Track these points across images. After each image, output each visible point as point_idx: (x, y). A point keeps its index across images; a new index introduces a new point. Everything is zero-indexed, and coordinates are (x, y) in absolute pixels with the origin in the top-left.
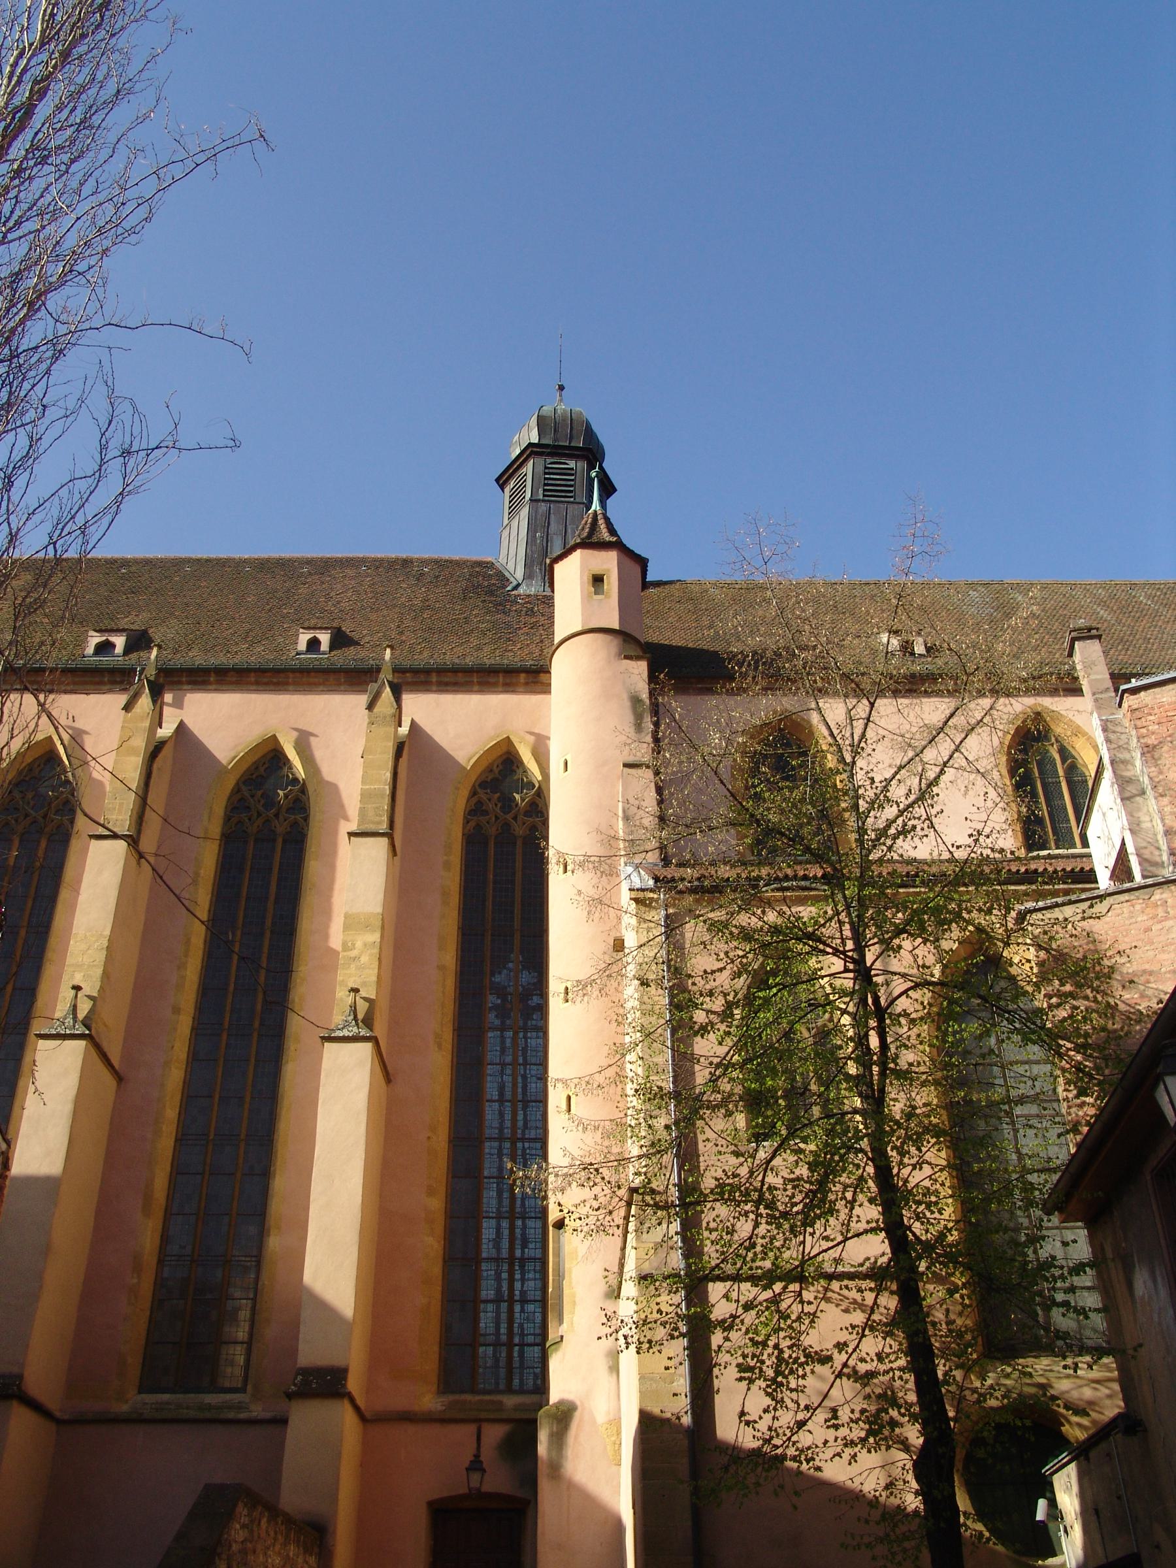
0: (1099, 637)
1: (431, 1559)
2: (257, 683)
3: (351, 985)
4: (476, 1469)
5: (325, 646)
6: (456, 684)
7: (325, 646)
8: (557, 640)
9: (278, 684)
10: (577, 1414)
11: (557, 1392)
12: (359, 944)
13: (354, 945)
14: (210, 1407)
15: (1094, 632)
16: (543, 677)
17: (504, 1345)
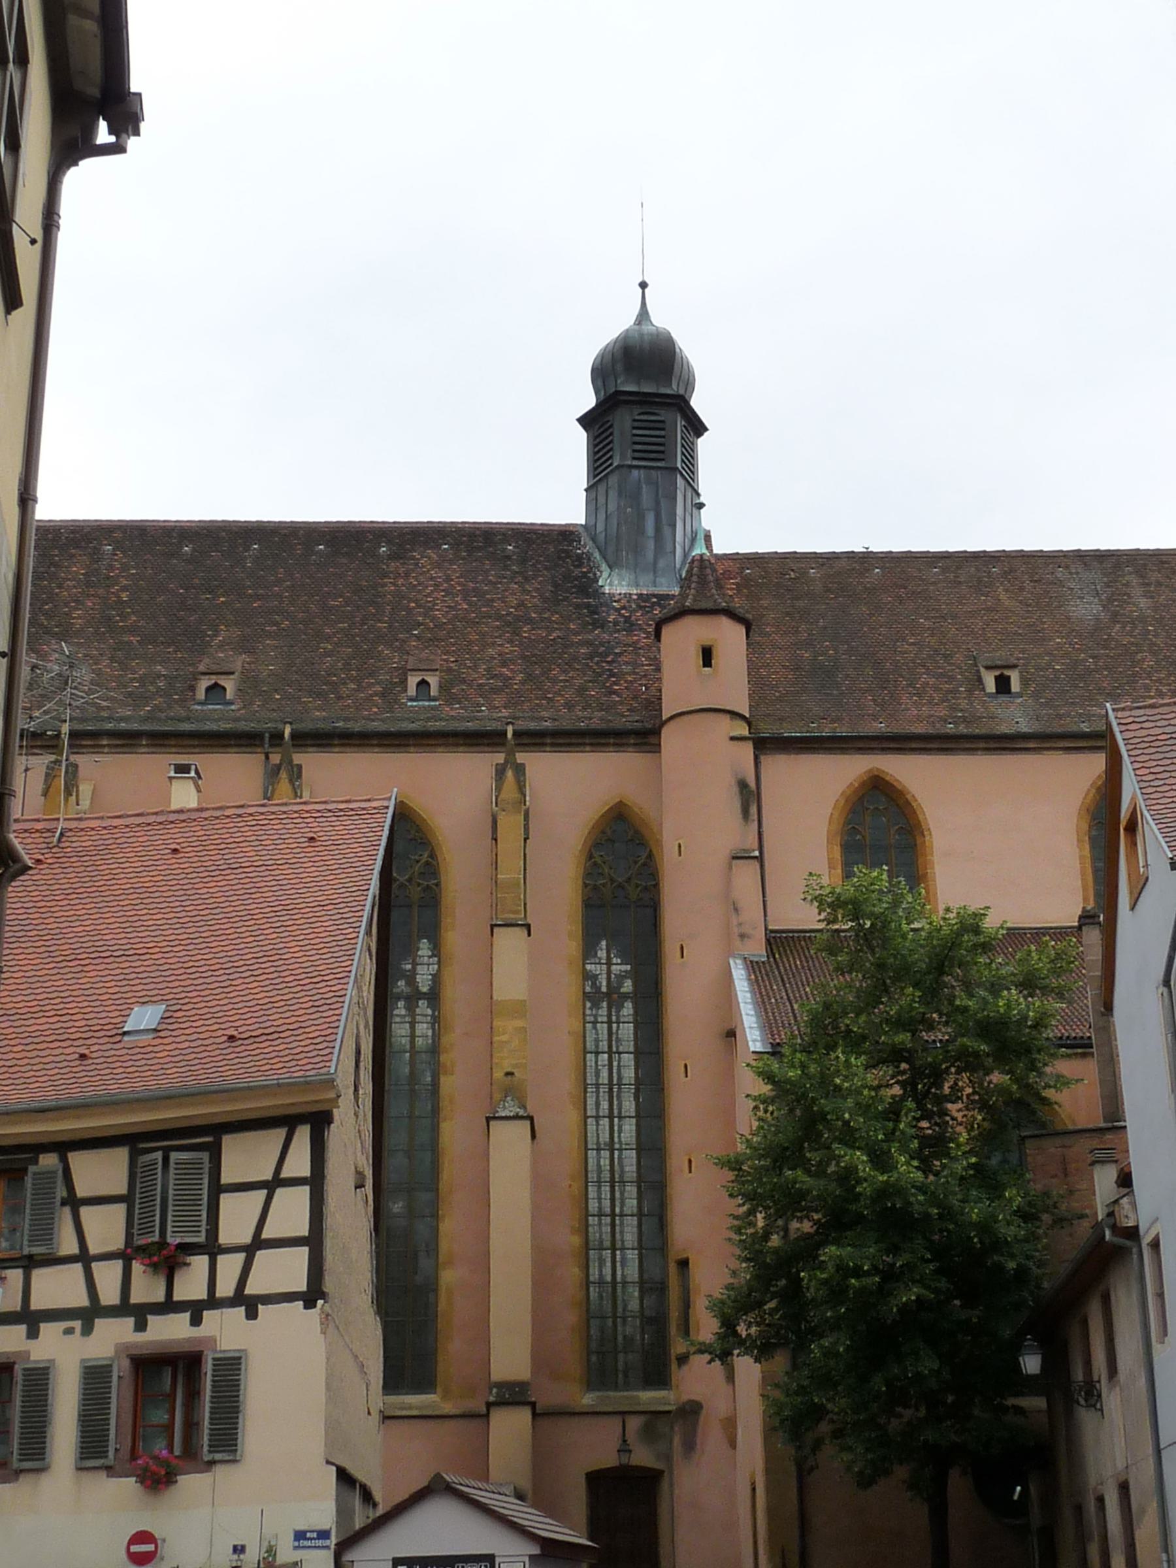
5: (434, 691)
6: (570, 745)
14: (410, 1408)
16: (653, 740)
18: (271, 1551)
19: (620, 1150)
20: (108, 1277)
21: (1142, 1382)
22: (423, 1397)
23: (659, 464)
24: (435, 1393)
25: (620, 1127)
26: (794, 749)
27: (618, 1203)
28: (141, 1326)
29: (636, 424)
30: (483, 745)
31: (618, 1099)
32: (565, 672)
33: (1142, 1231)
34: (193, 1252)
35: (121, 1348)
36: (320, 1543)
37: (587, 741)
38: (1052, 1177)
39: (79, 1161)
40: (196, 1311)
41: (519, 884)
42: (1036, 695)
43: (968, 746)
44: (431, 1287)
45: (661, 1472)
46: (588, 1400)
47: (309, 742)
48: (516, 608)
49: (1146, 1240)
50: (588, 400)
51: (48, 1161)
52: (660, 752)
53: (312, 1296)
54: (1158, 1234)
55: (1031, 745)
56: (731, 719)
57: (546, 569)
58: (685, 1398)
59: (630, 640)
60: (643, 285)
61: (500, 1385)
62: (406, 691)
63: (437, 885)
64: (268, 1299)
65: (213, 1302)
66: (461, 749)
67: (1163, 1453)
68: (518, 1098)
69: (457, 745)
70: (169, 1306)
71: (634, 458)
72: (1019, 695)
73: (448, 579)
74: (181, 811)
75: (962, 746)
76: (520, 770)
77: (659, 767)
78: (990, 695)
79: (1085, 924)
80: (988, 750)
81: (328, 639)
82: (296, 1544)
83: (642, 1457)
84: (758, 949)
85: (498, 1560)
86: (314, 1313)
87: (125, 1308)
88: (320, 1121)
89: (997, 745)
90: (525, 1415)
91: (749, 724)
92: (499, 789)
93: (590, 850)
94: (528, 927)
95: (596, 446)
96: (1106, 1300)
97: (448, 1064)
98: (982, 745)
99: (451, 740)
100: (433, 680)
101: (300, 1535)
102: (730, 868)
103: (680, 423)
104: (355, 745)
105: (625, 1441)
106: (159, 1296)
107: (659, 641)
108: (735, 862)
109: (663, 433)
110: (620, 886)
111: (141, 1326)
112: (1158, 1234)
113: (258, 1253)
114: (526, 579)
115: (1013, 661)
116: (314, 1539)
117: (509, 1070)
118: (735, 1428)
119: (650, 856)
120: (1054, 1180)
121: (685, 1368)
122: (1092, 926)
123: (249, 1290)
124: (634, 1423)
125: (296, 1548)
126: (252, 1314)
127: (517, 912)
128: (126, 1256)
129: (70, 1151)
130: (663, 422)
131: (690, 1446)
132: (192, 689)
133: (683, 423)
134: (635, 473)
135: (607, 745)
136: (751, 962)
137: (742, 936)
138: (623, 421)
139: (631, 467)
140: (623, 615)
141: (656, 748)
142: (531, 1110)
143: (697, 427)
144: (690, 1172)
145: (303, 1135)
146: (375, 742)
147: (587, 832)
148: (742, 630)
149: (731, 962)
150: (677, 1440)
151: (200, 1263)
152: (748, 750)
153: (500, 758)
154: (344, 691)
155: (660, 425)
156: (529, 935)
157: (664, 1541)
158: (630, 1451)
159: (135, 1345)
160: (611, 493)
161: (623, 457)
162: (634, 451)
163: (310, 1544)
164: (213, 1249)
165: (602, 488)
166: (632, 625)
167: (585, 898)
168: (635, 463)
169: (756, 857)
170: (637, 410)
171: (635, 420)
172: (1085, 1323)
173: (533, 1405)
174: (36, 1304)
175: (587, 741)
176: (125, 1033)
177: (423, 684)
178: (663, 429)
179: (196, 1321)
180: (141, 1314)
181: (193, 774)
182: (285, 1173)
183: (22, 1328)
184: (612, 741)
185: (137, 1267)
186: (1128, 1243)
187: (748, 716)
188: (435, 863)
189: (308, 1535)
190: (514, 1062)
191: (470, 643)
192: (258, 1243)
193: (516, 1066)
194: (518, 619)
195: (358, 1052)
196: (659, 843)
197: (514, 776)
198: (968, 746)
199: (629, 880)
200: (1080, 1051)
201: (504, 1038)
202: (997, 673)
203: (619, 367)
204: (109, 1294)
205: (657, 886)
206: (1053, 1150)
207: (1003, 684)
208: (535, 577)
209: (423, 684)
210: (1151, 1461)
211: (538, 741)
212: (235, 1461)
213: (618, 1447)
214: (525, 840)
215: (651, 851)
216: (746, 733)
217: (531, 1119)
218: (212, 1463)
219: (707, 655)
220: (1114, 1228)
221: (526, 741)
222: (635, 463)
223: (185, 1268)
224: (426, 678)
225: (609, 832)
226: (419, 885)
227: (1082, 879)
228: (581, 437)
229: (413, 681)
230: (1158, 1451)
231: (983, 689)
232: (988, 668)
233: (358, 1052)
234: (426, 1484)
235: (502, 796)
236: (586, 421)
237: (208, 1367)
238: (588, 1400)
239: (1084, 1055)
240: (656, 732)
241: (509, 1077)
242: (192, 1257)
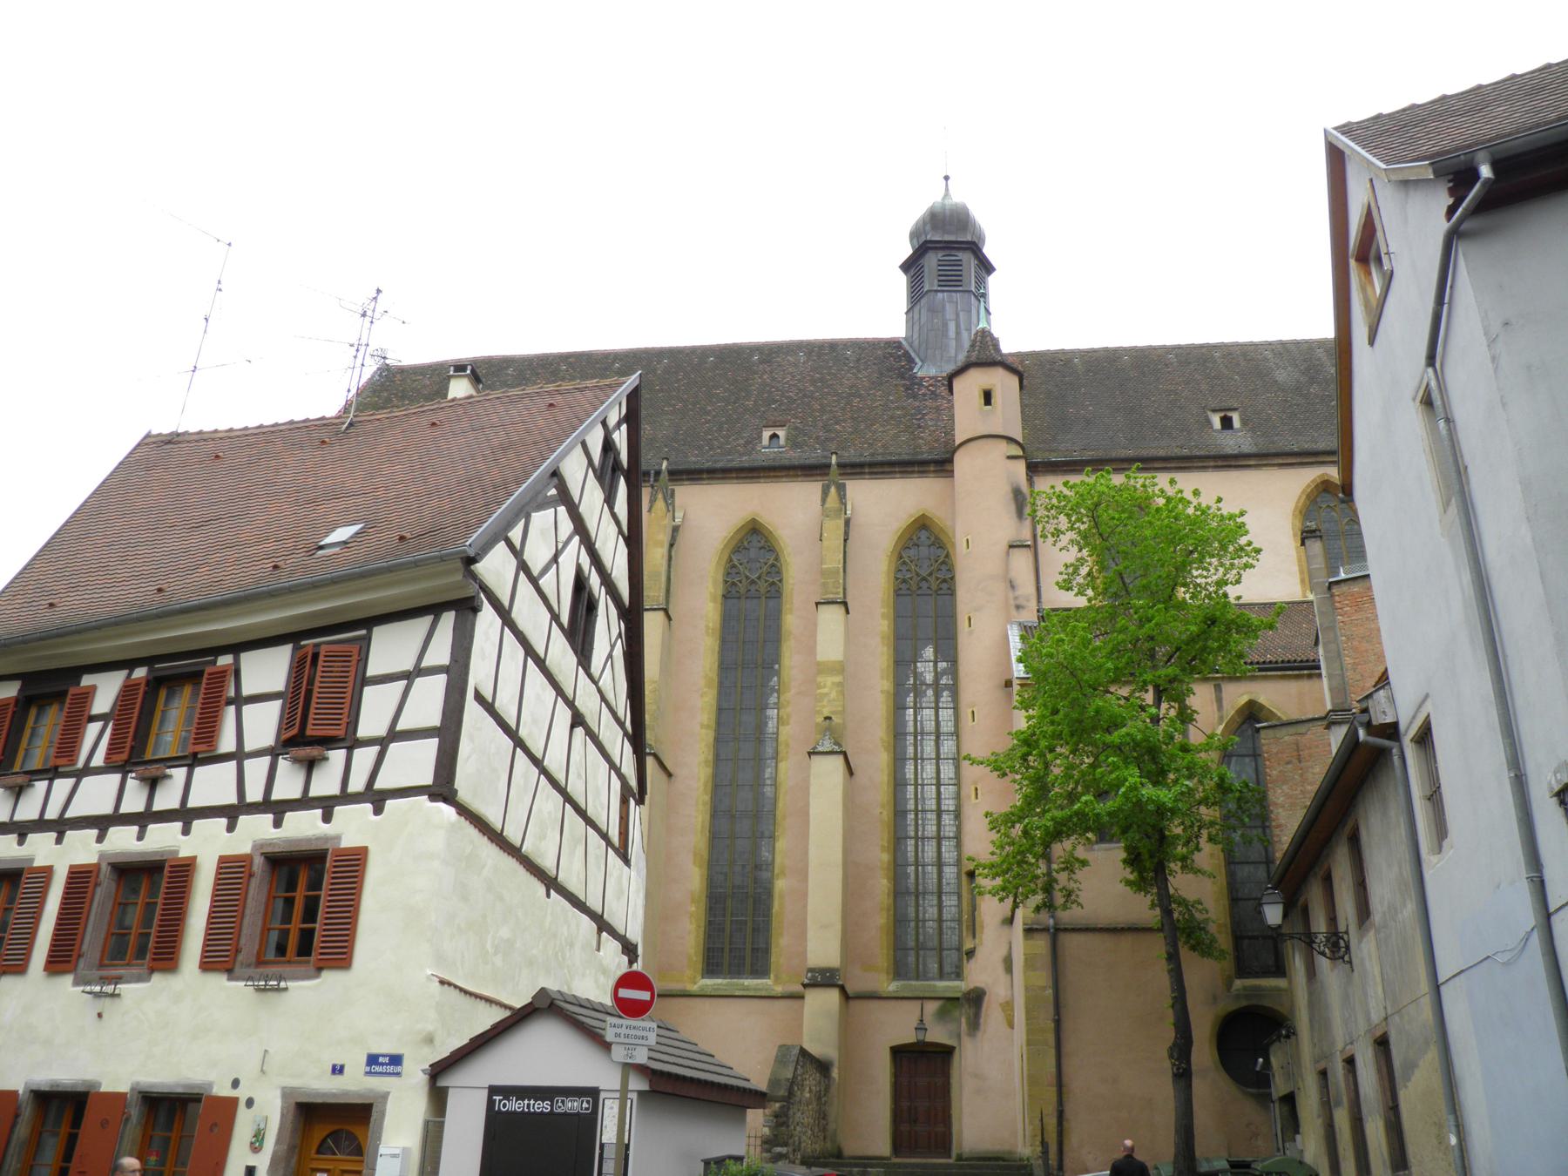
0: (1321, 537)
1: (893, 1080)
2: (737, 478)
3: (826, 714)
4: (921, 1029)
5: (782, 441)
6: (883, 473)
7: (782, 441)
8: (957, 443)
9: (753, 478)
10: (986, 998)
11: (123, 988)
12: (829, 684)
13: (825, 684)
14: (747, 989)
15: (1318, 533)
16: (948, 467)
17: (912, 949)
19: (923, 785)
20: (256, 770)
21: (1410, 909)
22: (759, 981)
23: (960, 289)
24: (769, 978)
25: (922, 767)
26: (1061, 471)
27: (920, 828)
28: (277, 824)
29: (940, 263)
30: (817, 475)
32: (883, 426)
33: (1402, 727)
34: (332, 746)
35: (257, 846)
36: (390, 1069)
37: (897, 470)
38: (1288, 763)
39: (249, 660)
40: (327, 806)
41: (838, 572)
42: (1253, 430)
43: (1200, 464)
44: (769, 893)
45: (953, 1048)
46: (893, 987)
47: (684, 477)
49: (1409, 733)
50: (906, 251)
52: (953, 477)
53: (442, 789)
54: (1429, 715)
55: (1252, 463)
56: (1007, 443)
57: (874, 364)
59: (934, 405)
60: (947, 178)
61: (811, 970)
62: (761, 443)
63: (780, 581)
65: (345, 798)
66: (799, 479)
67: (1443, 989)
68: (834, 738)
69: (798, 476)
70: (304, 802)
71: (939, 286)
72: (1239, 430)
74: (453, 400)
75: (1195, 465)
76: (841, 489)
77: (953, 486)
78: (1216, 431)
79: (1307, 538)
80: (1217, 468)
81: (708, 413)
82: (368, 1069)
83: (938, 1034)
84: (1030, 617)
85: (603, 1095)
89: (1225, 464)
90: (833, 996)
91: (1023, 449)
92: (824, 500)
93: (900, 553)
94: (845, 604)
95: (912, 287)
96: (1355, 841)
97: (785, 717)
98: (1212, 464)
99: (791, 473)
100: (781, 433)
101: (372, 1060)
102: (1008, 554)
103: (974, 262)
104: (719, 479)
105: (922, 1021)
106: (295, 793)
107: (952, 394)
108: (1011, 550)
109: (960, 268)
110: (924, 579)
111: (277, 824)
112: (1429, 715)
113: (392, 745)
114: (859, 371)
115: (1236, 405)
116: (386, 1064)
117: (829, 715)
118: (1012, 1010)
119: (947, 556)
120: (1290, 766)
121: (972, 962)
122: (1313, 540)
124: (931, 1007)
125: (368, 1073)
126: (378, 810)
127: (838, 593)
128: (274, 753)
129: (243, 652)
130: (960, 260)
131: (975, 1025)
133: (976, 262)
134: (940, 295)
135: (913, 472)
136: (1025, 627)
137: (1018, 607)
138: (932, 261)
139: (937, 291)
140: (930, 390)
141: (950, 473)
143: (986, 267)
144: (977, 798)
146: (734, 475)
147: (896, 538)
148: (1014, 381)
149: (1009, 627)
151: (337, 756)
152: (1020, 468)
155: (958, 263)
156: (847, 612)
158: (926, 1029)
159: (270, 843)
160: (922, 311)
161: (931, 285)
162: (939, 281)
163: (381, 1070)
164: (352, 743)
165: (916, 309)
166: (936, 396)
167: (896, 588)
168: (939, 288)
169: (1029, 546)
170: (940, 255)
171: (939, 260)
172: (1328, 880)
173: (842, 989)
174: (192, 803)
175: (897, 470)
176: (321, 548)
177: (774, 436)
178: (961, 265)
179: (327, 818)
180: (277, 809)
181: (468, 372)
182: (425, 663)
183: (178, 825)
184: (916, 469)
185: (283, 764)
186: (1386, 743)
187: (1021, 442)
188: (778, 564)
189: (381, 1060)
190: (834, 709)
191: (814, 410)
192: (394, 735)
193: (834, 712)
194: (851, 395)
196: (953, 545)
197: (837, 491)
198: (1200, 464)
199: (930, 574)
200: (1306, 672)
201: (825, 690)
202: (1222, 414)
203: (928, 227)
204: (254, 794)
205: (952, 578)
206: (1286, 738)
207: (1227, 423)
208: (866, 369)
209: (774, 436)
210: (1427, 1003)
211: (858, 470)
212: (398, 1074)
213: (915, 1025)
214: (845, 540)
215: (948, 552)
216: (1021, 453)
217: (845, 754)
219: (988, 397)
220: (1368, 725)
221: (849, 471)
222: (939, 288)
223: (323, 763)
224: (777, 432)
225: (915, 538)
226: (766, 581)
227: (1299, 565)
228: (902, 280)
229: (766, 434)
230: (1437, 988)
231: (1212, 428)
232: (1214, 411)
234: (530, 1000)
235: (827, 505)
236: (906, 267)
238: (893, 987)
239: (1310, 676)
240: (950, 461)
241: (828, 721)
242: (330, 752)
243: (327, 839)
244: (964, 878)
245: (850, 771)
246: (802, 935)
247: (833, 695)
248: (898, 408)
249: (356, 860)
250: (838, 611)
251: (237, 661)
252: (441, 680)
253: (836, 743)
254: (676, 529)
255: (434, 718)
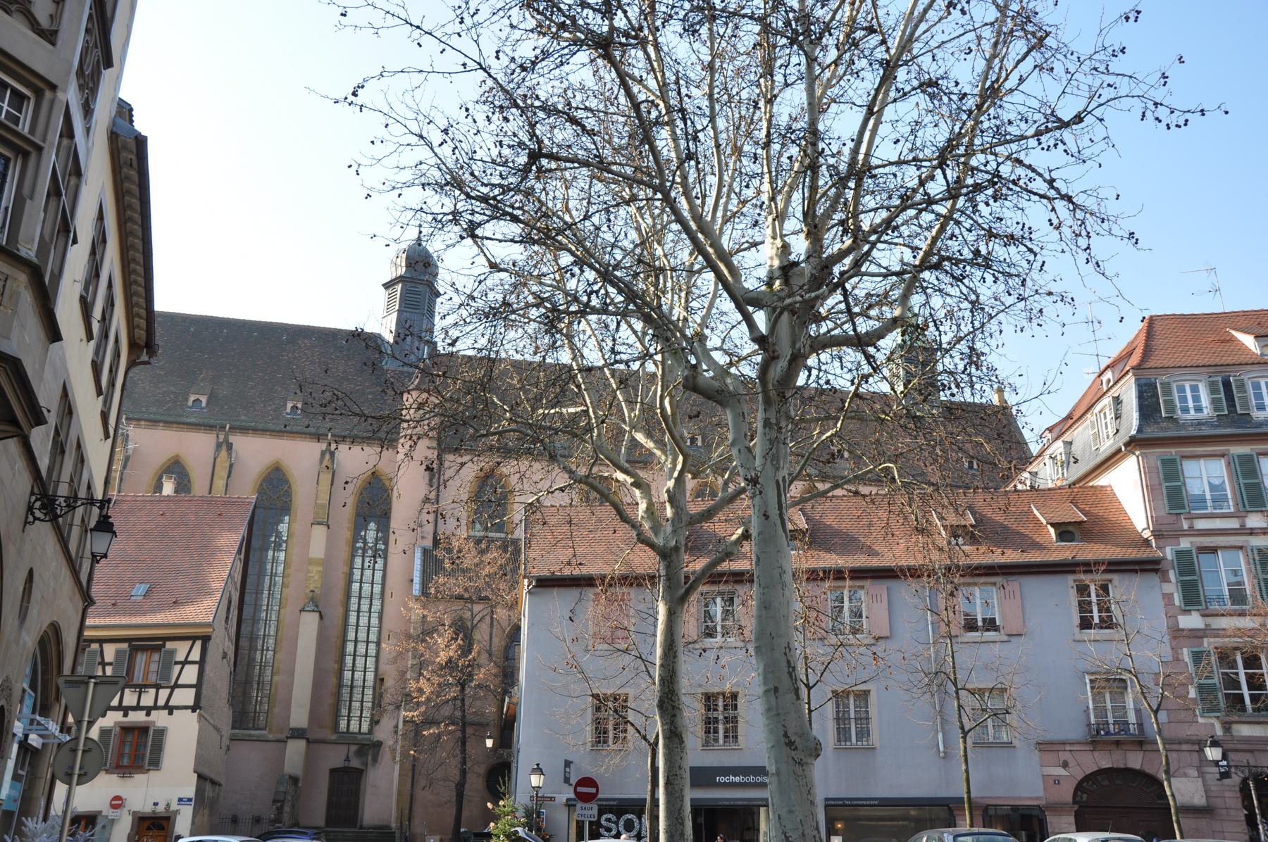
18: (168, 805)
28: (126, 715)
31: (722, 261)
35: (116, 723)
40: (148, 710)
48: (343, 373)
51: (95, 646)
58: (376, 739)
61: (291, 729)
64: (178, 708)
65: (156, 707)
70: (138, 708)
73: (313, 356)
83: (355, 763)
86: (195, 714)
87: (120, 707)
88: (206, 639)
90: (301, 744)
92: (321, 462)
101: (180, 800)
106: (135, 704)
111: (126, 715)
123: (171, 703)
124: (354, 748)
126: (171, 713)
131: (375, 760)
132: (187, 400)
142: (320, 609)
145: (198, 644)
150: (370, 758)
153: (324, 446)
154: (257, 408)
157: (361, 800)
159: (123, 722)
179: (148, 714)
180: (126, 710)
182: (189, 659)
195: (230, 602)
218: (149, 770)
233: (230, 602)
237: (151, 732)
243: (149, 722)
244: (378, 681)
245: (321, 617)
246: (288, 706)
247: (316, 578)
248: (369, 393)
249: (161, 734)
250: (324, 528)
251: (101, 647)
252: (196, 667)
253: (317, 606)
254: (231, 466)
255: (194, 682)
